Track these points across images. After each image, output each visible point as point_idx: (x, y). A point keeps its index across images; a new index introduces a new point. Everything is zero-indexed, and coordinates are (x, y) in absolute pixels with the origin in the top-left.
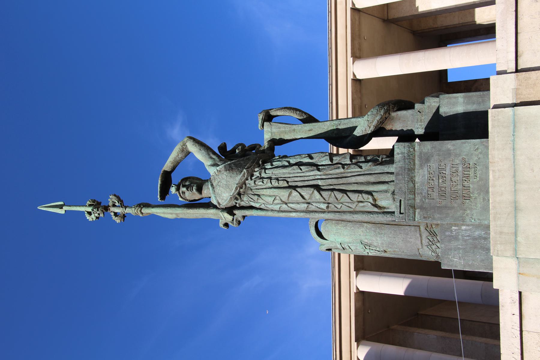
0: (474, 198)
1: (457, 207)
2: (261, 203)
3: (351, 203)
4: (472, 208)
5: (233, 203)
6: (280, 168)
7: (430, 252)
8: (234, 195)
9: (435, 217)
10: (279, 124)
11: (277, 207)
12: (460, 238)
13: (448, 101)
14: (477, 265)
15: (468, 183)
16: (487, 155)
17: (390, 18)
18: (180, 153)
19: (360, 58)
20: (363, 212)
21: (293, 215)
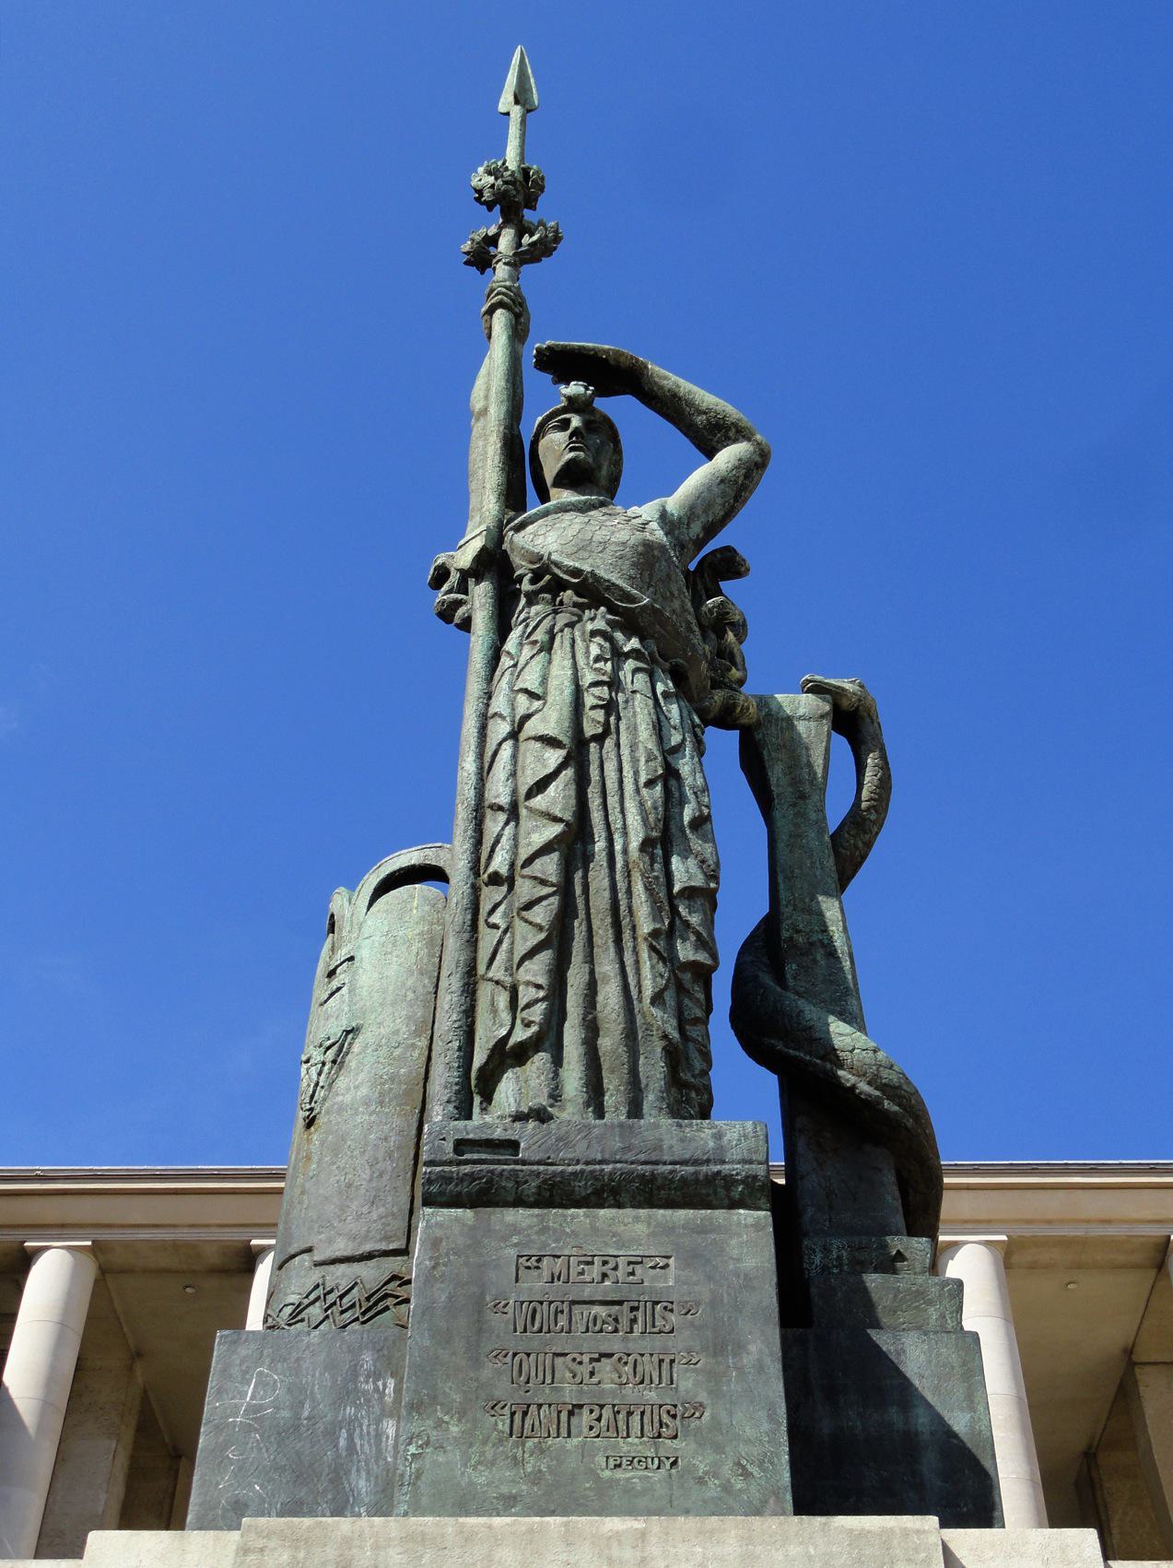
0: (519, 1454)
1: (477, 1380)
2: (519, 656)
3: (510, 959)
4: (471, 1445)
5: (522, 567)
6: (654, 717)
7: (294, 1299)
8: (553, 567)
9: (438, 1285)
10: (824, 744)
11: (499, 704)
12: (345, 1409)
13: (953, 1368)
14: (218, 1484)
15: (586, 1430)
16: (720, 1508)
17: (1137, 1370)
18: (708, 420)
19: (1006, 1268)
20: (470, 1013)
21: (469, 765)
